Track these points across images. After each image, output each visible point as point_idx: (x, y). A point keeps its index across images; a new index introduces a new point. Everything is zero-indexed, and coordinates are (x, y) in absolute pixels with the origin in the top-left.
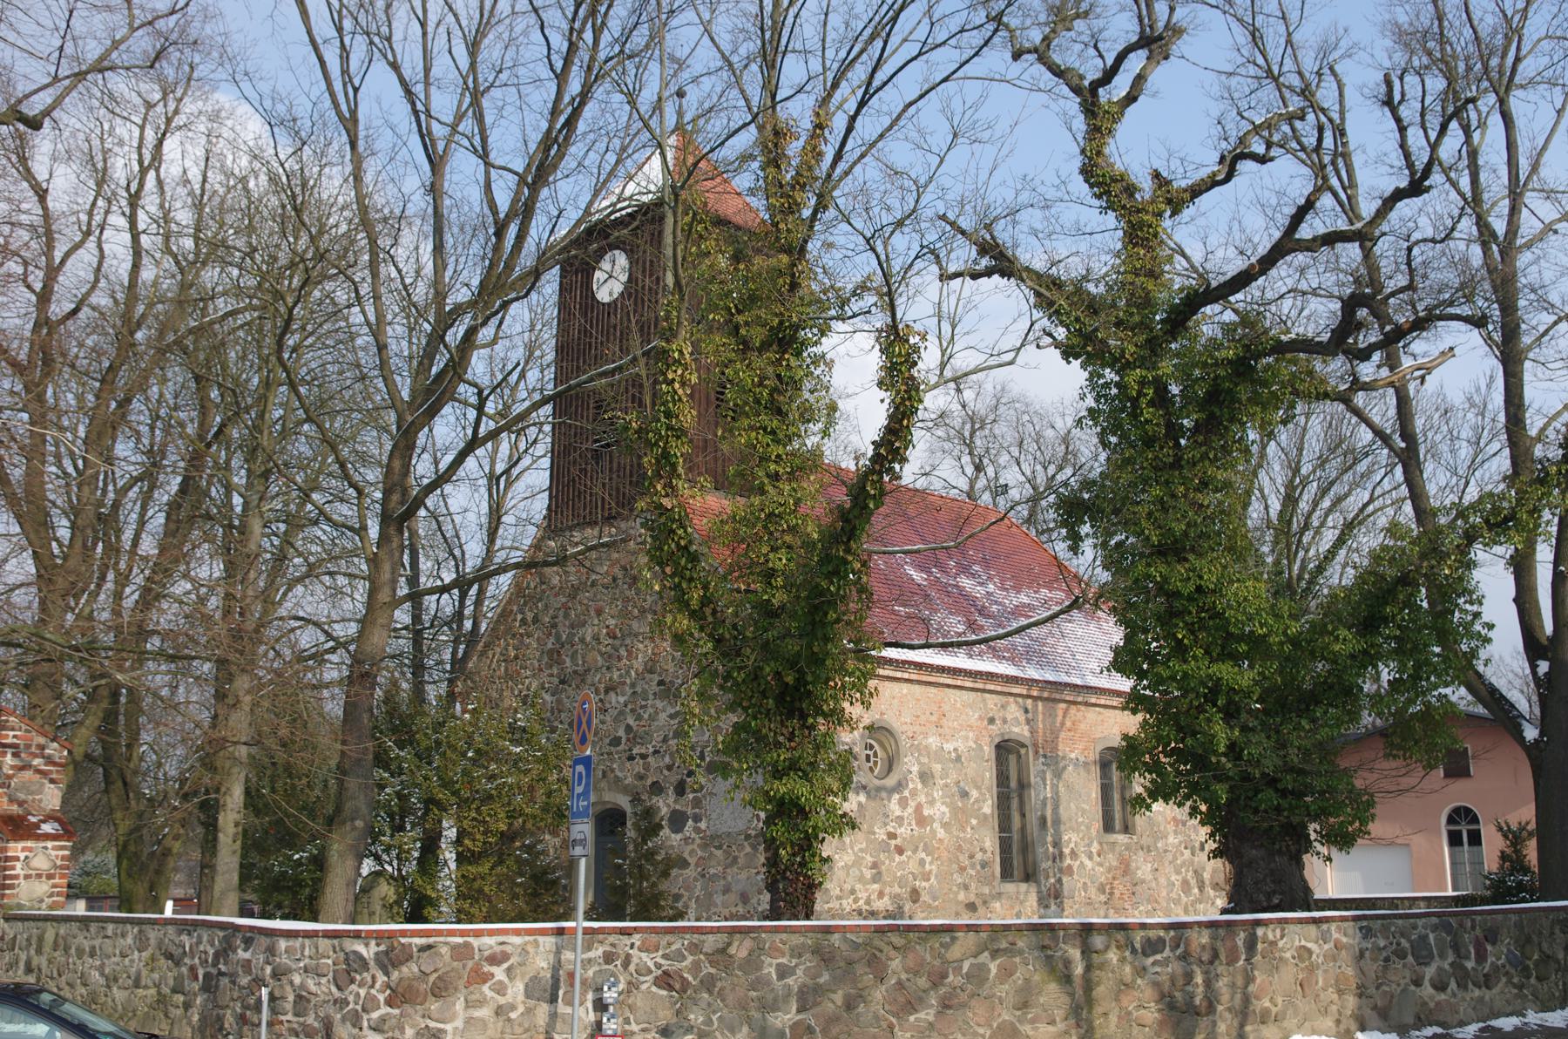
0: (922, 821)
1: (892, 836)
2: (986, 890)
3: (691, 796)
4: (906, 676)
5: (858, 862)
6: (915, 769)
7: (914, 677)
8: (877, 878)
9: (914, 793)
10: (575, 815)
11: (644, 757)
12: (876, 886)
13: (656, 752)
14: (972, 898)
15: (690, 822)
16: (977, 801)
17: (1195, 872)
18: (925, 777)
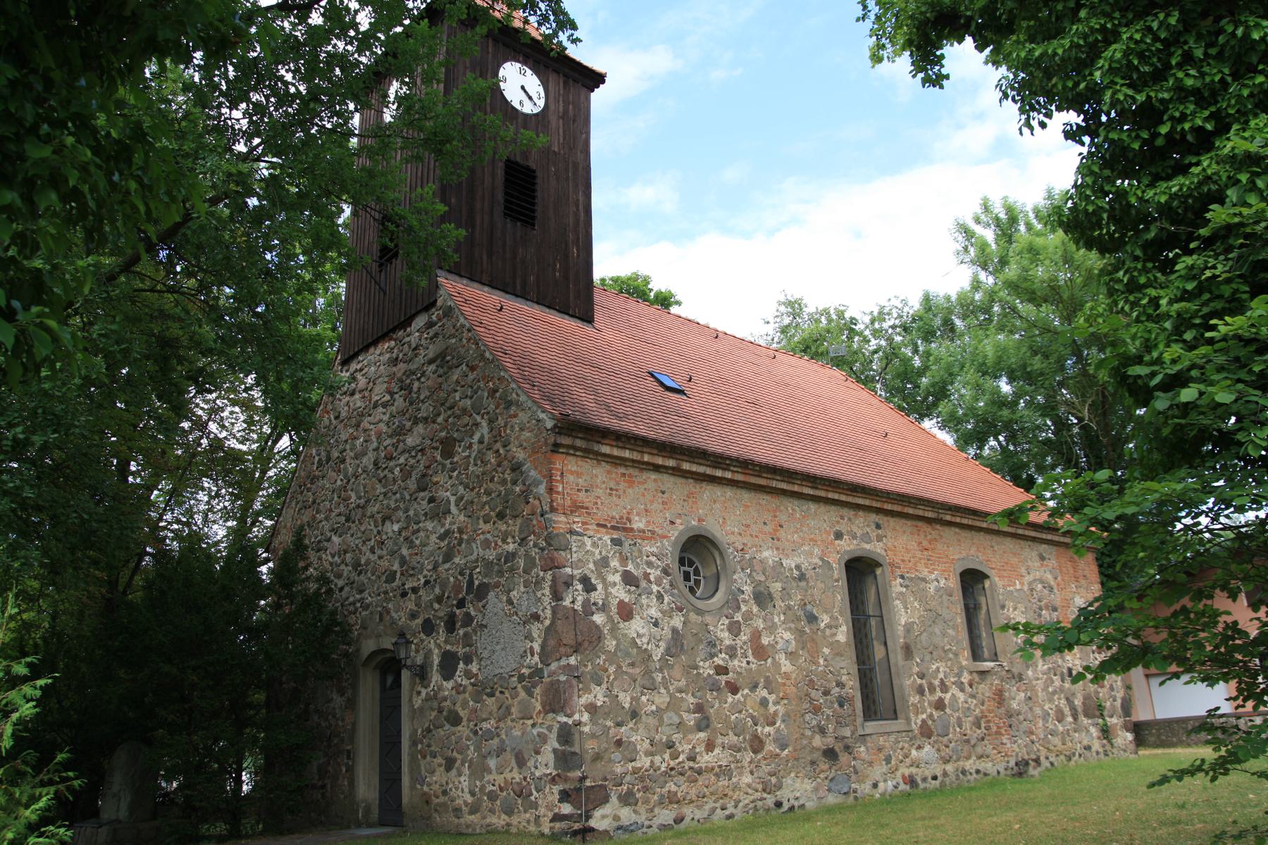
0: (761, 652)
1: (722, 670)
2: (847, 732)
3: (461, 632)
4: (728, 475)
5: (674, 705)
6: (748, 589)
7: (739, 477)
8: (704, 724)
9: (748, 616)
10: (818, 749)
11: (415, 590)
12: (702, 735)
13: (427, 582)
14: (830, 741)
15: (461, 665)
16: (829, 626)
17: (1067, 699)
18: (763, 598)
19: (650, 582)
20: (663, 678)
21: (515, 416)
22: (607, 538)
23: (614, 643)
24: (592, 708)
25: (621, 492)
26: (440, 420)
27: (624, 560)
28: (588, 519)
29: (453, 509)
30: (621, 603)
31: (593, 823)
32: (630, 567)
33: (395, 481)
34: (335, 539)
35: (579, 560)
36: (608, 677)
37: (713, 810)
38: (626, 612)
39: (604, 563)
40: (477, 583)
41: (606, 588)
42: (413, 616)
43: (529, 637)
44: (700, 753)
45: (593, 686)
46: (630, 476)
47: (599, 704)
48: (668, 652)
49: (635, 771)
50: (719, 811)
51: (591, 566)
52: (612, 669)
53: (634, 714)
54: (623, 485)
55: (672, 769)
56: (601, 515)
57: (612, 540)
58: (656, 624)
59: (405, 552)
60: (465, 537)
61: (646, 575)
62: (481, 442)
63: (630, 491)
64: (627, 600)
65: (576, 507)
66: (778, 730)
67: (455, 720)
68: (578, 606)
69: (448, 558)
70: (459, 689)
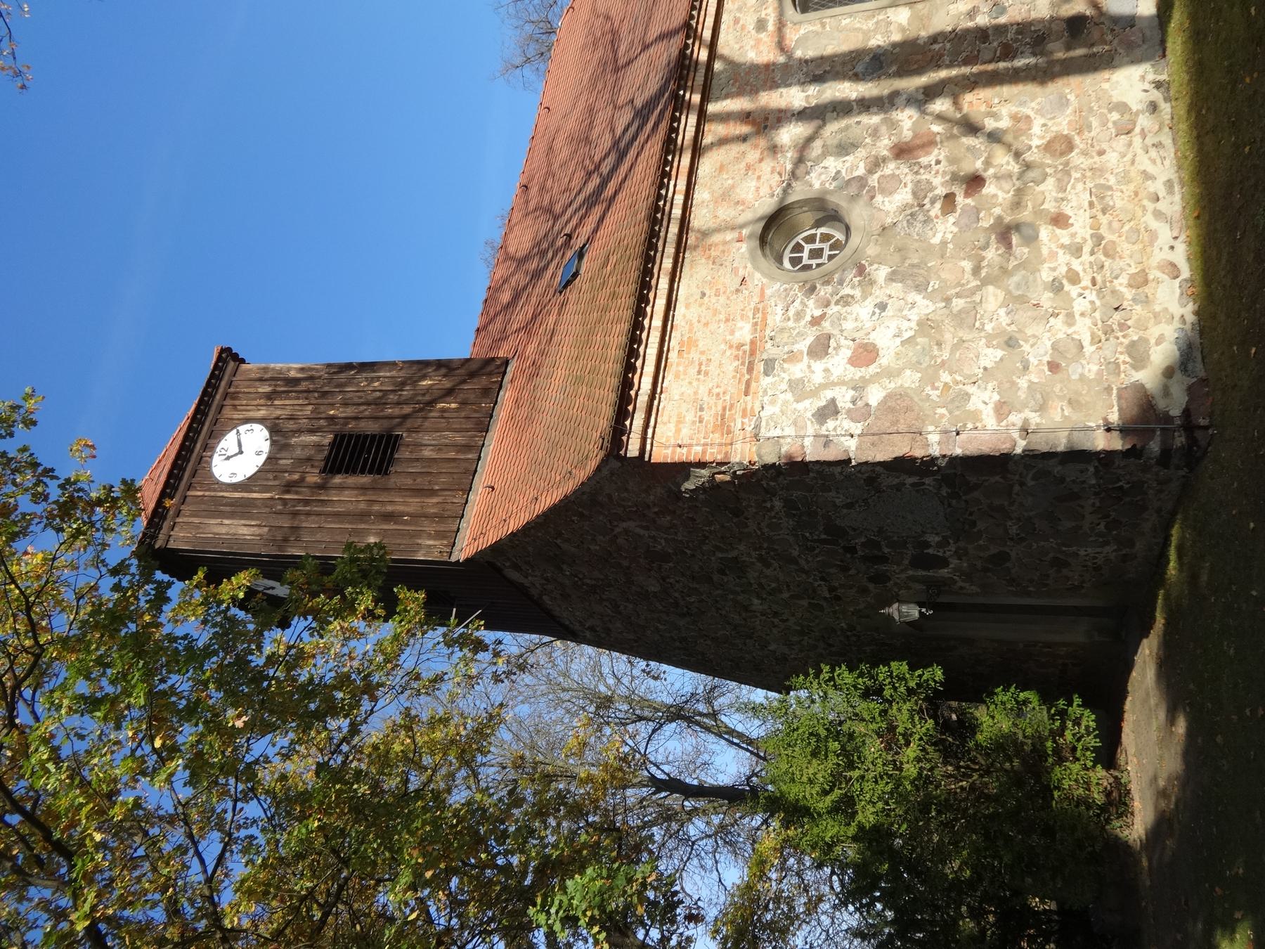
3: (886, 550)
13: (822, 579)
19: (823, 316)
20: (958, 295)
21: (610, 496)
22: (766, 381)
23: (908, 372)
24: (1002, 410)
25: (704, 358)
26: (625, 563)
27: (792, 357)
28: (739, 407)
29: (734, 554)
30: (855, 361)
31: (1176, 412)
32: (803, 346)
33: (701, 601)
34: (772, 647)
35: (795, 423)
36: (957, 383)
37: (1158, 214)
38: (866, 353)
39: (798, 388)
40: (823, 536)
41: (834, 384)
42: (864, 591)
43: (899, 487)
44: (1073, 235)
45: (971, 406)
46: (681, 343)
47: (996, 397)
48: (920, 288)
49: (1095, 340)
50: (1161, 206)
51: (800, 406)
52: (945, 377)
53: (1011, 343)
54: (694, 355)
55: (1094, 282)
56: (733, 388)
57: (766, 374)
58: (882, 307)
59: (786, 595)
60: (765, 545)
61: (816, 321)
62: (647, 528)
63: (701, 344)
64: (849, 353)
65: (723, 424)
66: (1039, 112)
67: (1002, 557)
68: (857, 428)
69: (794, 561)
70: (959, 555)
